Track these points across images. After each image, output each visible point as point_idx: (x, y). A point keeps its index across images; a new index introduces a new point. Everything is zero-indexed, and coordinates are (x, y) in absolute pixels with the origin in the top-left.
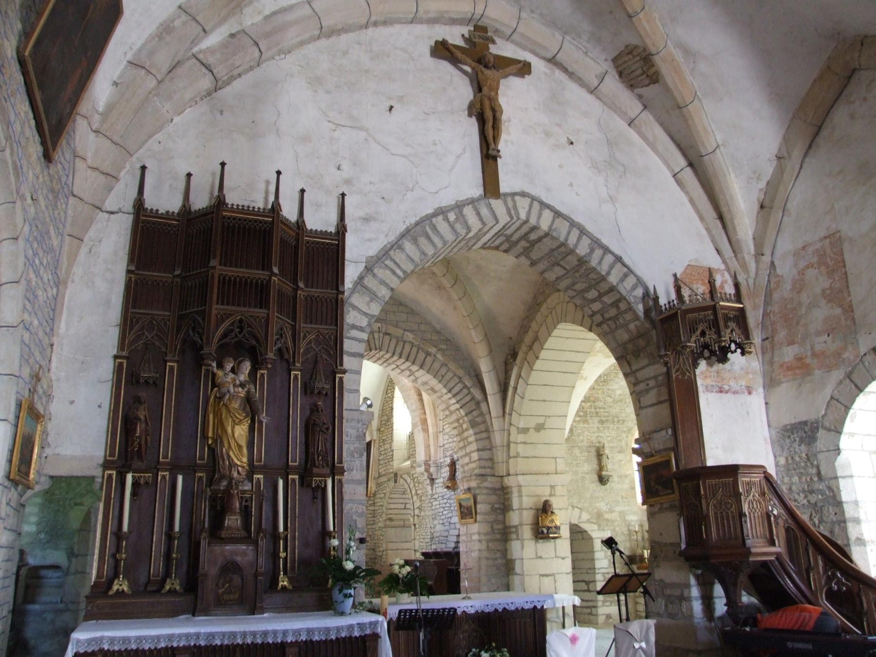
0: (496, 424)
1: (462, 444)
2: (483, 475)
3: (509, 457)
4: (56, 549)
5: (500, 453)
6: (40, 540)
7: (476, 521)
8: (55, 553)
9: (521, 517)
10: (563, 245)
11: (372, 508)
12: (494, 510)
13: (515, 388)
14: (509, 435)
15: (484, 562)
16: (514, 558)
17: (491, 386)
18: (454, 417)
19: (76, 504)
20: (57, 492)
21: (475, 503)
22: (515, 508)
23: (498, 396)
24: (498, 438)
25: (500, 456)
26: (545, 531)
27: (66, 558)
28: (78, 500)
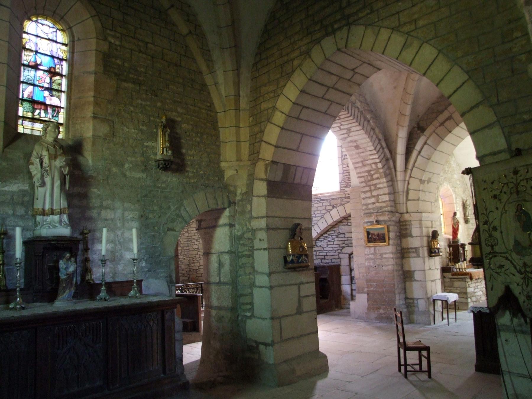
0: (400, 176)
1: (367, 189)
2: (392, 212)
3: (407, 200)
4: (157, 278)
5: (401, 197)
6: (142, 268)
7: (389, 244)
8: (157, 281)
9: (417, 241)
10: (97, 38)
11: (187, 234)
12: (397, 236)
13: (420, 152)
14: (408, 184)
15: (396, 273)
16: (413, 269)
17: (401, 148)
18: (367, 168)
19: (169, 230)
20: (151, 216)
21: (389, 231)
22: (414, 234)
23: (404, 157)
24: (400, 186)
25: (402, 198)
26: (437, 251)
27: (167, 286)
28: (170, 226)
